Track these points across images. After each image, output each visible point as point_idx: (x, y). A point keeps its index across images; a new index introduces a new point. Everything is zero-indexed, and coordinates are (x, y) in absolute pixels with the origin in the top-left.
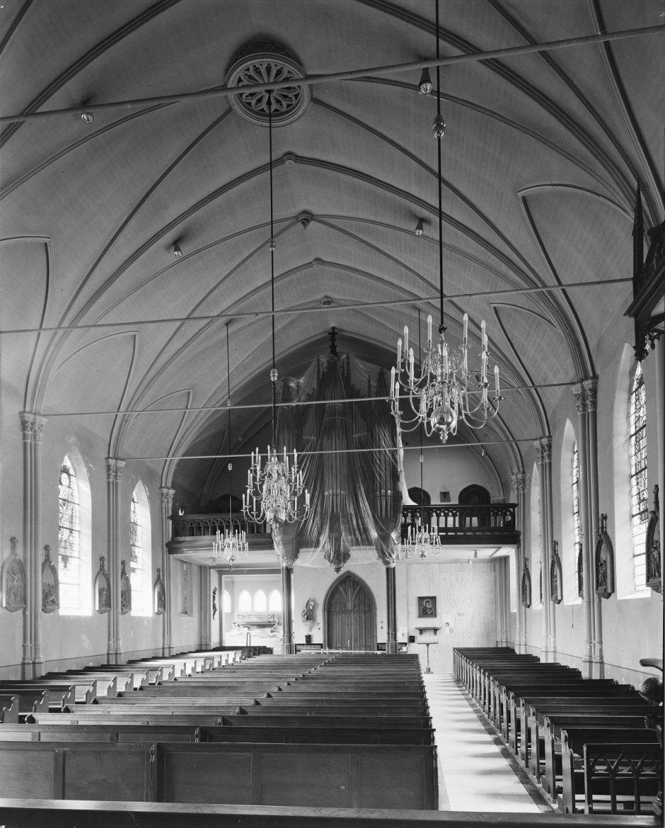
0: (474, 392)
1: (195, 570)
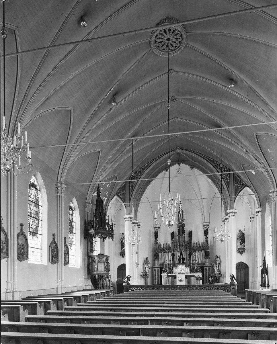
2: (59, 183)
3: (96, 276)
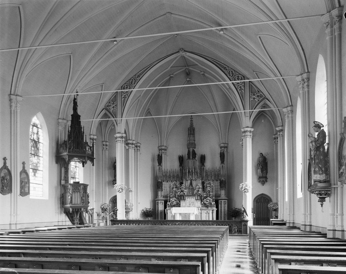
2: (13, 95)
3: (70, 210)
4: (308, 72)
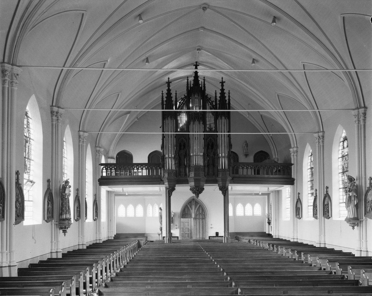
0: (278, 111)
1: (277, 192)
2: (82, 131)
4: (323, 131)
